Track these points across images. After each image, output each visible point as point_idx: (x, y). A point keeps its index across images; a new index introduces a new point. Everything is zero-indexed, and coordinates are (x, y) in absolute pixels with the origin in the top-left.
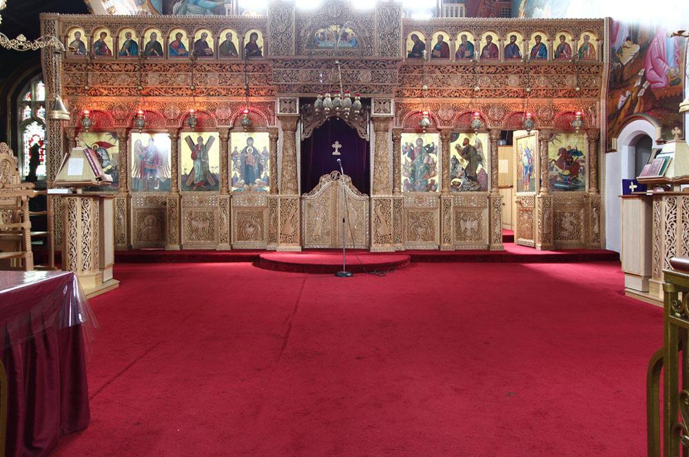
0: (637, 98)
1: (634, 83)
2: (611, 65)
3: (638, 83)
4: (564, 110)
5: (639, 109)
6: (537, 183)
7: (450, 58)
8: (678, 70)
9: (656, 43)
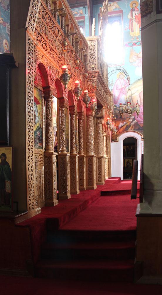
0: (130, 125)
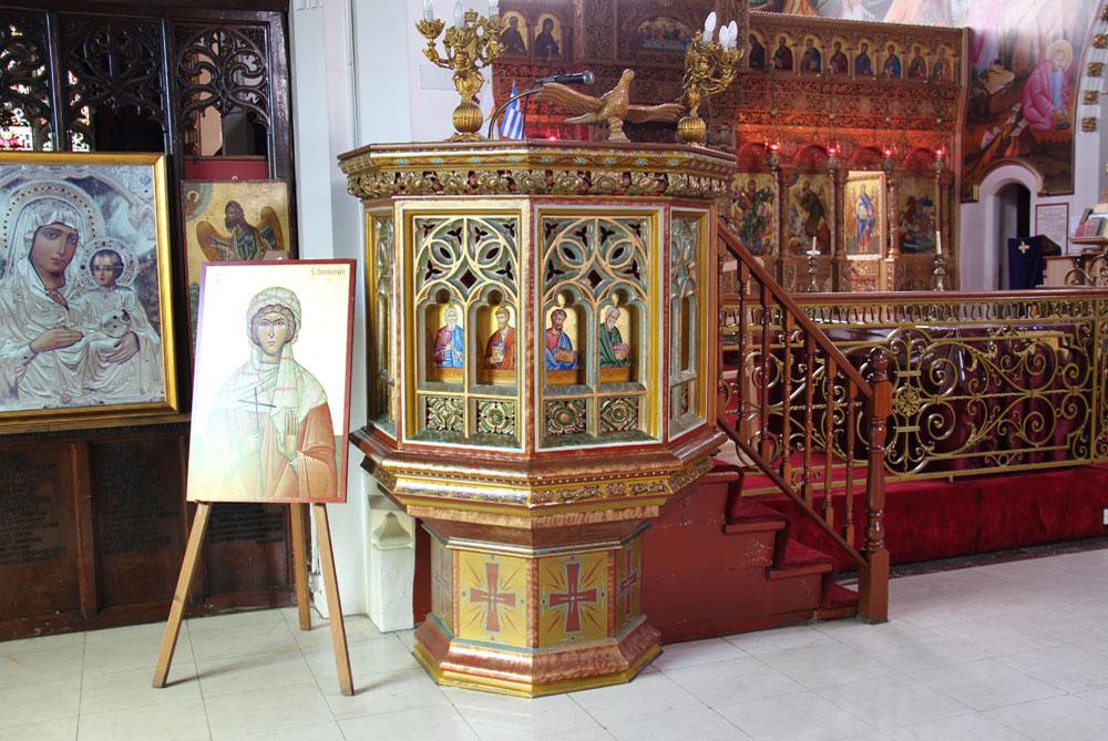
0: (1010, 138)
1: (1006, 119)
2: (970, 91)
3: (1012, 120)
4: (918, 145)
5: (1013, 150)
6: (882, 243)
7: (794, 71)
8: (1066, 113)
9: (1038, 76)
